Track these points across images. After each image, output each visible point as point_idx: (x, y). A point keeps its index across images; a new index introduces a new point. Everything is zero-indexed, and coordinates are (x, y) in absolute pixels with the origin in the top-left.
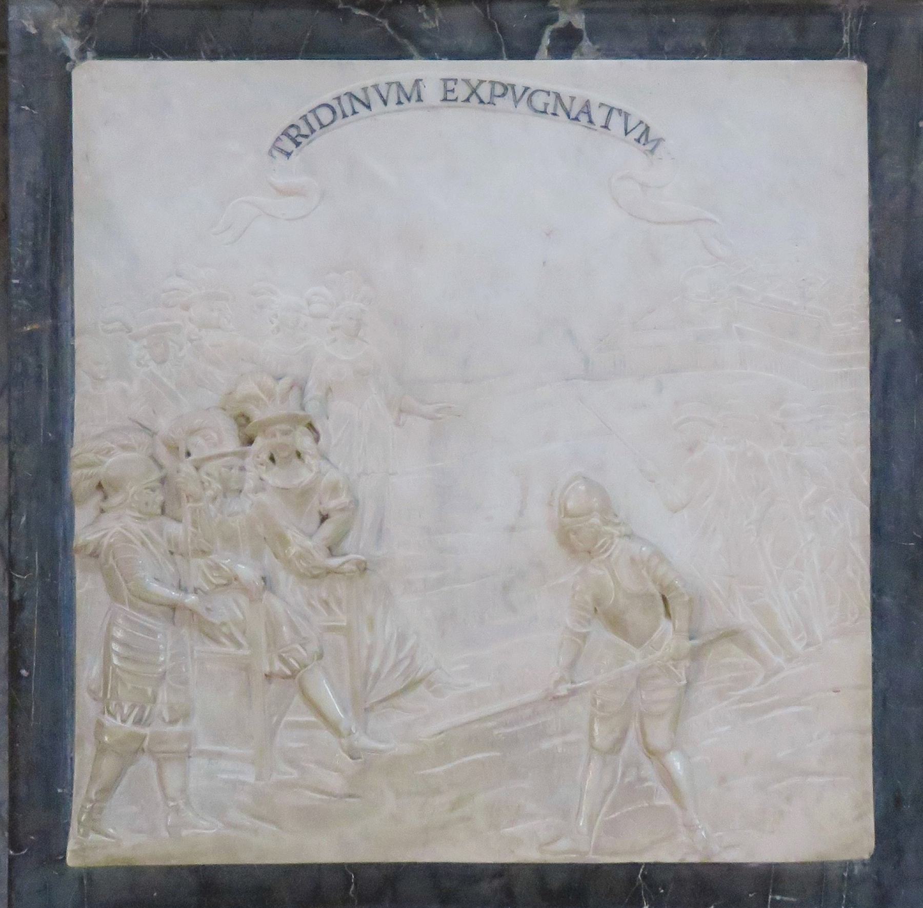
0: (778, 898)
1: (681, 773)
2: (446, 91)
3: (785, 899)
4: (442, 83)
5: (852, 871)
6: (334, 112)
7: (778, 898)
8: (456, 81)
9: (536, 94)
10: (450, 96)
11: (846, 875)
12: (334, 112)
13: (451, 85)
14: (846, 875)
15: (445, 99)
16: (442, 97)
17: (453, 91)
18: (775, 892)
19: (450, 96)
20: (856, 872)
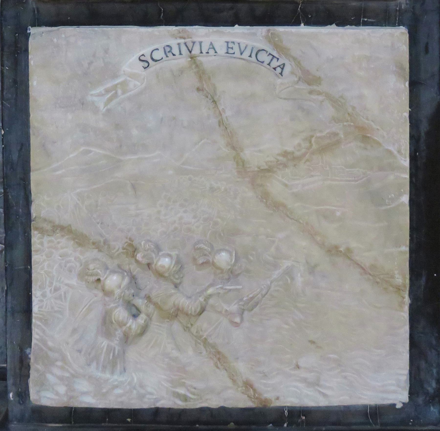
0: (366, 20)
1: (279, 29)
2: (228, 48)
3: (369, 20)
4: (226, 44)
5: (401, 7)
6: (152, 59)
7: (366, 20)
8: (233, 43)
9: (261, 52)
10: (231, 51)
11: (398, 9)
12: (152, 59)
13: (230, 45)
14: (398, 9)
15: (227, 53)
16: (226, 51)
17: (232, 48)
18: (364, 17)
19: (231, 51)
20: (403, 7)
